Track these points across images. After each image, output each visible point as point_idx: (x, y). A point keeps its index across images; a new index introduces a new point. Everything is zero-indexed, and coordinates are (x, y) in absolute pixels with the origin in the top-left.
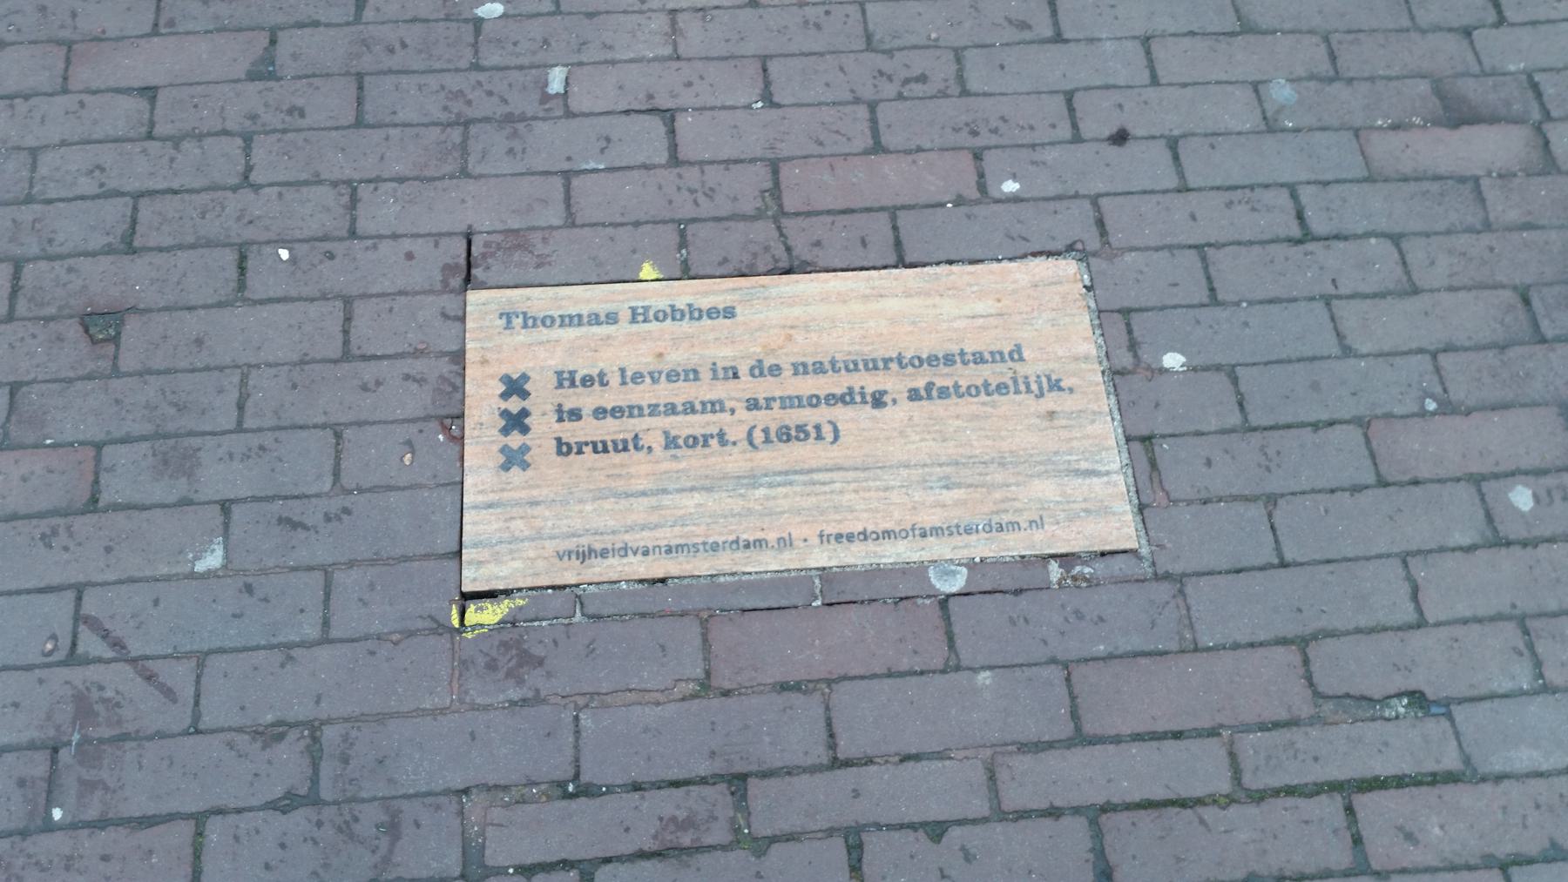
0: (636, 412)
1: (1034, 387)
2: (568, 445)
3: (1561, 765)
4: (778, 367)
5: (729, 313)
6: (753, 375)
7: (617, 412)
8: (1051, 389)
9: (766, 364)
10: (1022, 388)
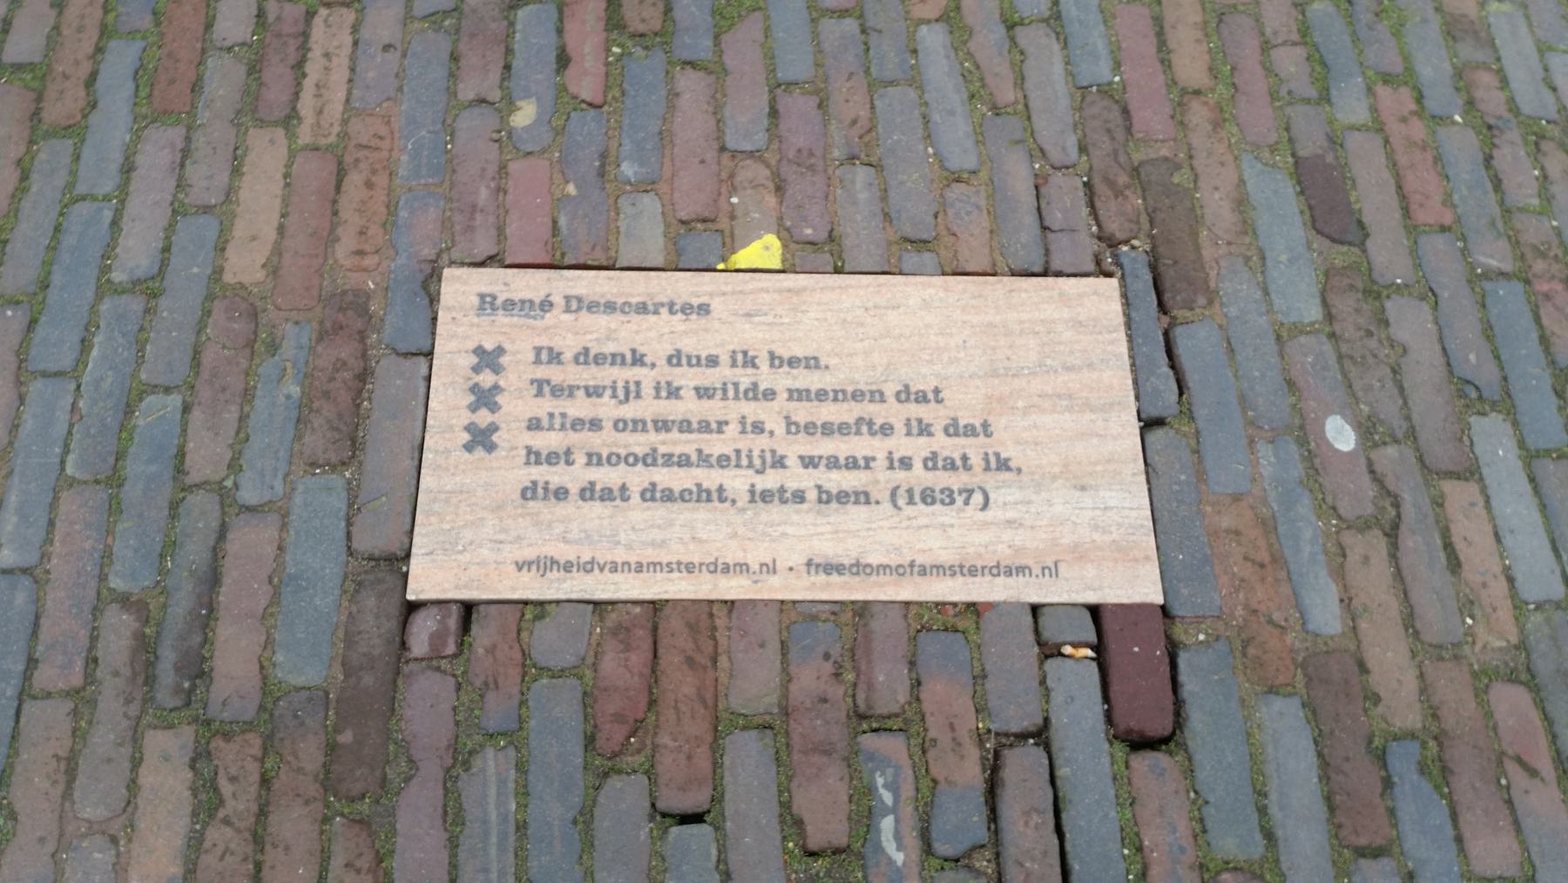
0: (862, 499)
1: (757, 462)
2: (780, 358)
3: (1007, 877)
4: (774, 393)
5: (704, 309)
6: (899, 401)
7: (685, 426)
8: (773, 466)
9: (762, 387)
10: (745, 462)
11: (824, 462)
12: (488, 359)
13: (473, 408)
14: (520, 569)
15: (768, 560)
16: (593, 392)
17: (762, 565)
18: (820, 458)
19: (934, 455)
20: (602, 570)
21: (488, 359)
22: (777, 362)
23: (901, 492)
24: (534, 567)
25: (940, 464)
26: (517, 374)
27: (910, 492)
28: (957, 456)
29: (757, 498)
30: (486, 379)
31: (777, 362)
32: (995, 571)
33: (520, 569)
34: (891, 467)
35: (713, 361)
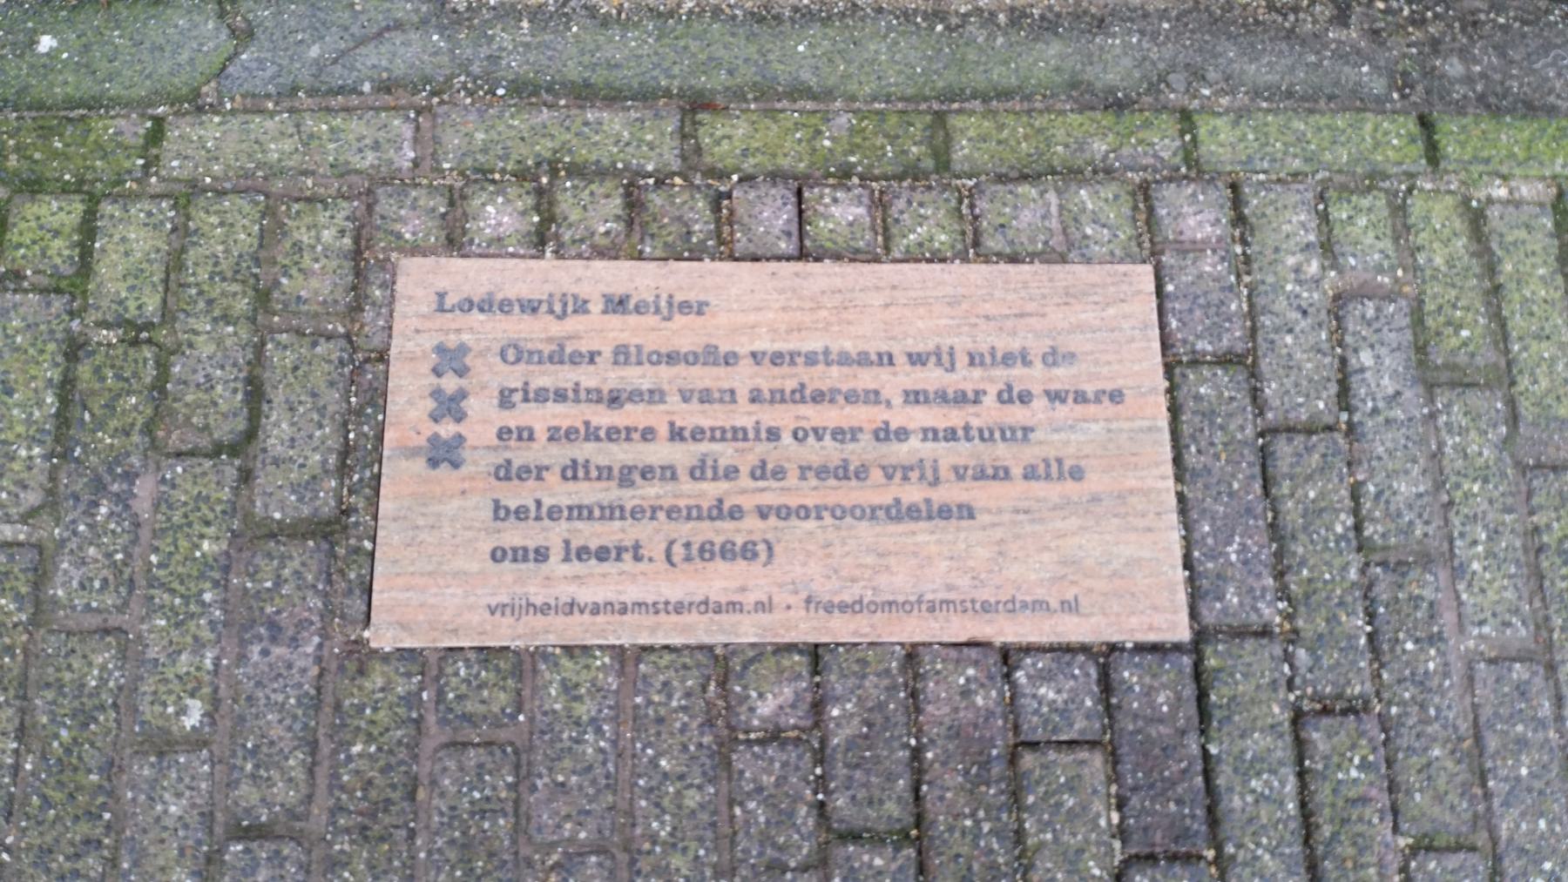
14: (493, 613)
15: (765, 599)
16: (622, 355)
17: (1062, 603)
20: (582, 612)
22: (502, 513)
24: (508, 611)
26: (491, 374)
29: (573, 556)
30: (450, 383)
31: (502, 513)
32: (703, 608)
33: (493, 613)
34: (567, 559)
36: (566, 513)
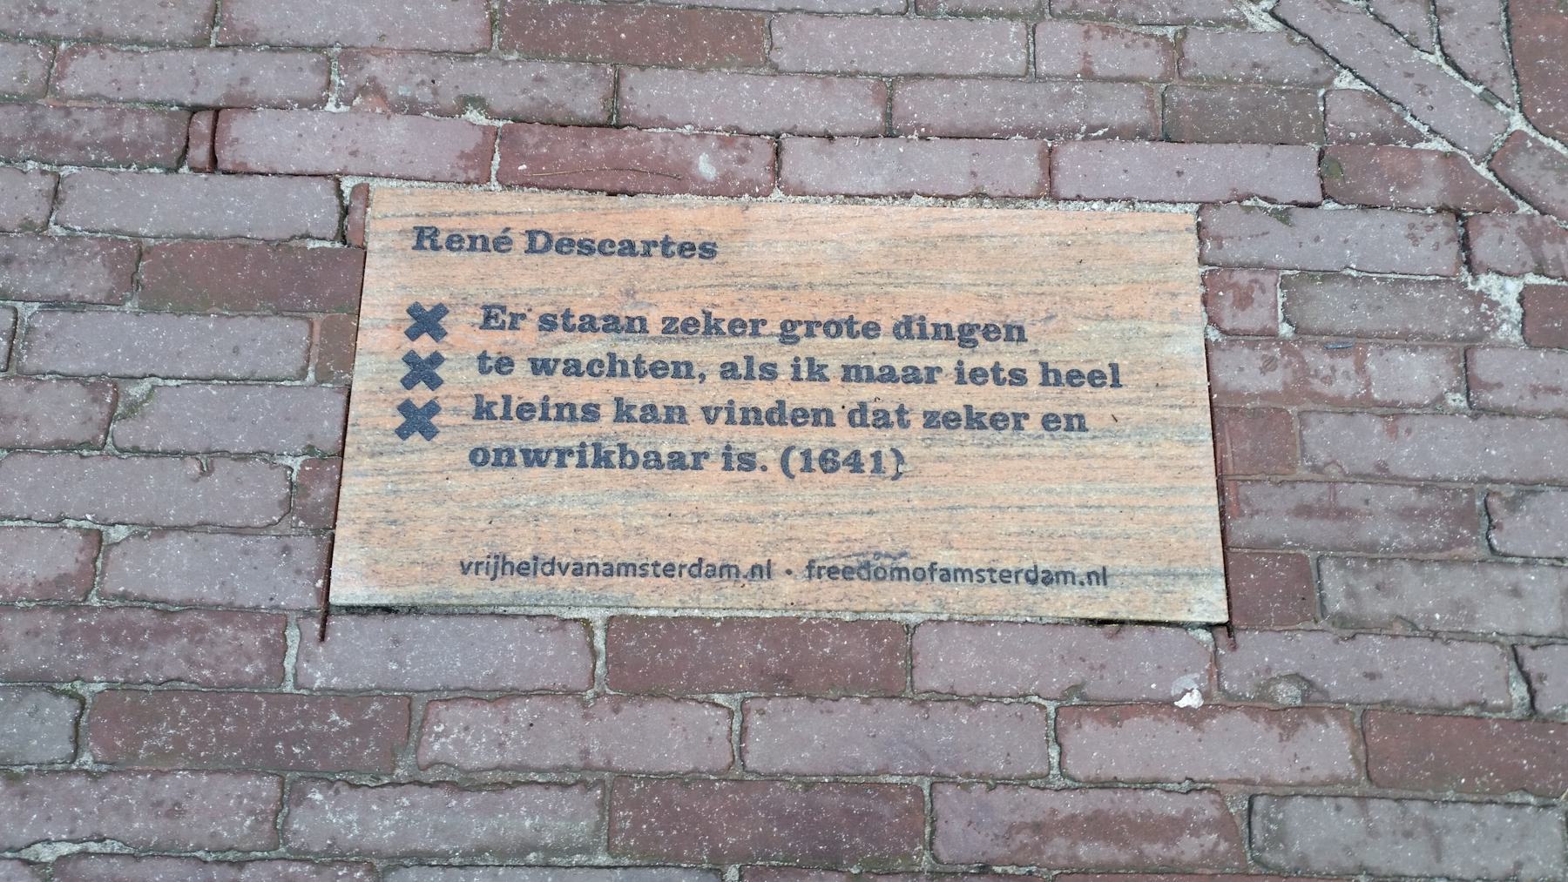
11: (561, 367)
12: (426, 321)
13: (408, 383)
18: (556, 361)
19: (863, 407)
21: (426, 321)
23: (795, 454)
25: (870, 418)
27: (806, 454)
28: (892, 408)
35: (871, 330)
36: (1064, 424)
